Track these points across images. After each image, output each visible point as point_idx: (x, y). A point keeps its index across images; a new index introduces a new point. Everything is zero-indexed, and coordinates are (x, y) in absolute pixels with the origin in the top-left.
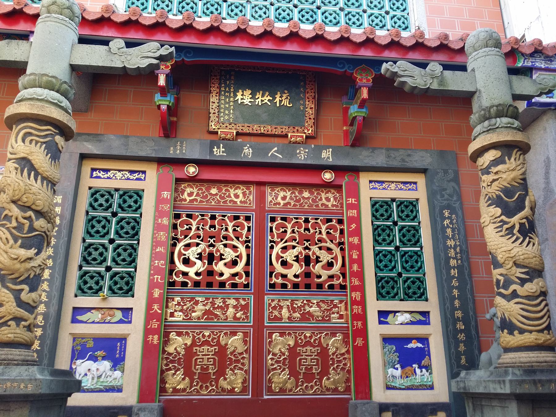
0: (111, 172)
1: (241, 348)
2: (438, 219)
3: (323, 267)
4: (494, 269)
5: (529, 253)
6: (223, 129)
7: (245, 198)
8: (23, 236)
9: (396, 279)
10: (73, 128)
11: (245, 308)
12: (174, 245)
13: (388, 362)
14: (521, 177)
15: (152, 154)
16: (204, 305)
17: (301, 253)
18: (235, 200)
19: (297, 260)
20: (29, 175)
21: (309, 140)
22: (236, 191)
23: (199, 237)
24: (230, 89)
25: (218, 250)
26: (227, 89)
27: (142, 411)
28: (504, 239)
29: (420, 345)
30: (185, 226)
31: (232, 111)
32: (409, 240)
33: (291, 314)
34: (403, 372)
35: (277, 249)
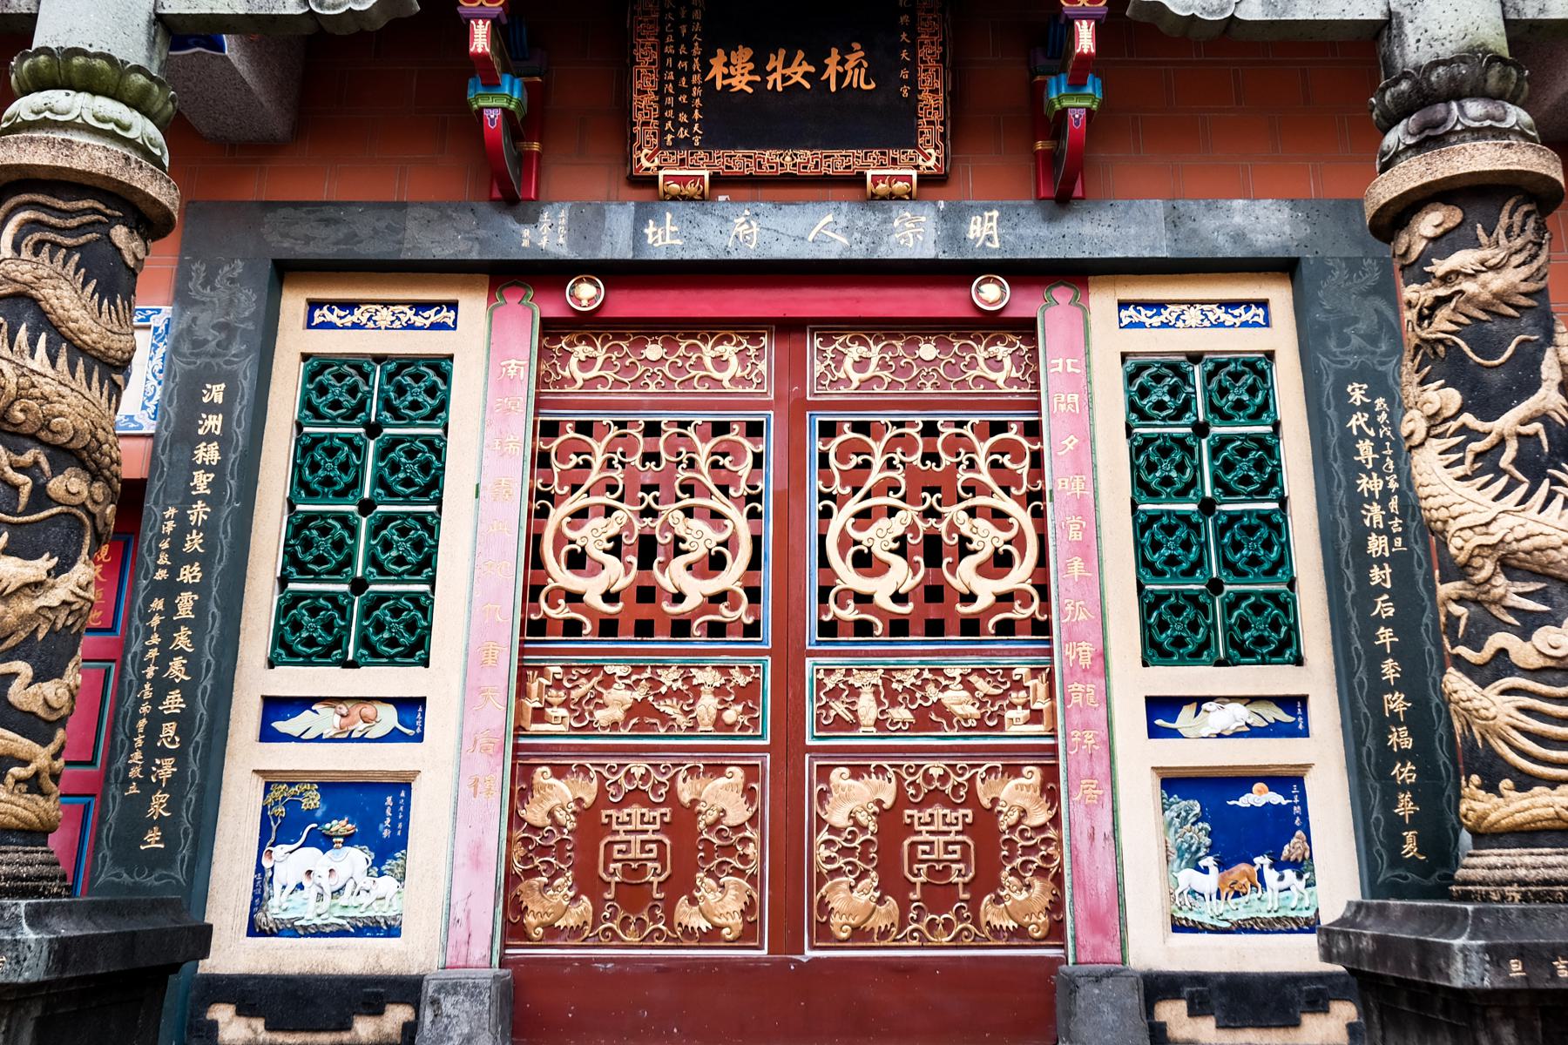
0: (363, 308)
1: (738, 812)
2: (1331, 412)
3: (981, 570)
4: (1442, 582)
5: (1547, 530)
6: (671, 168)
7: (744, 368)
8: (15, 519)
9: (1201, 599)
10: (162, 199)
11: (748, 694)
12: (543, 513)
13: (1179, 849)
14: (1531, 286)
15: (470, 251)
16: (628, 687)
17: (913, 527)
18: (716, 375)
19: (902, 548)
20: (33, 344)
21: (927, 191)
22: (720, 348)
23: (612, 488)
24: (690, 47)
25: (667, 527)
26: (682, 50)
27: (448, 993)
28: (1468, 489)
29: (1276, 799)
30: (573, 456)
31: (697, 115)
32: (1246, 480)
33: (882, 713)
34: (1222, 881)
35: (842, 518)
